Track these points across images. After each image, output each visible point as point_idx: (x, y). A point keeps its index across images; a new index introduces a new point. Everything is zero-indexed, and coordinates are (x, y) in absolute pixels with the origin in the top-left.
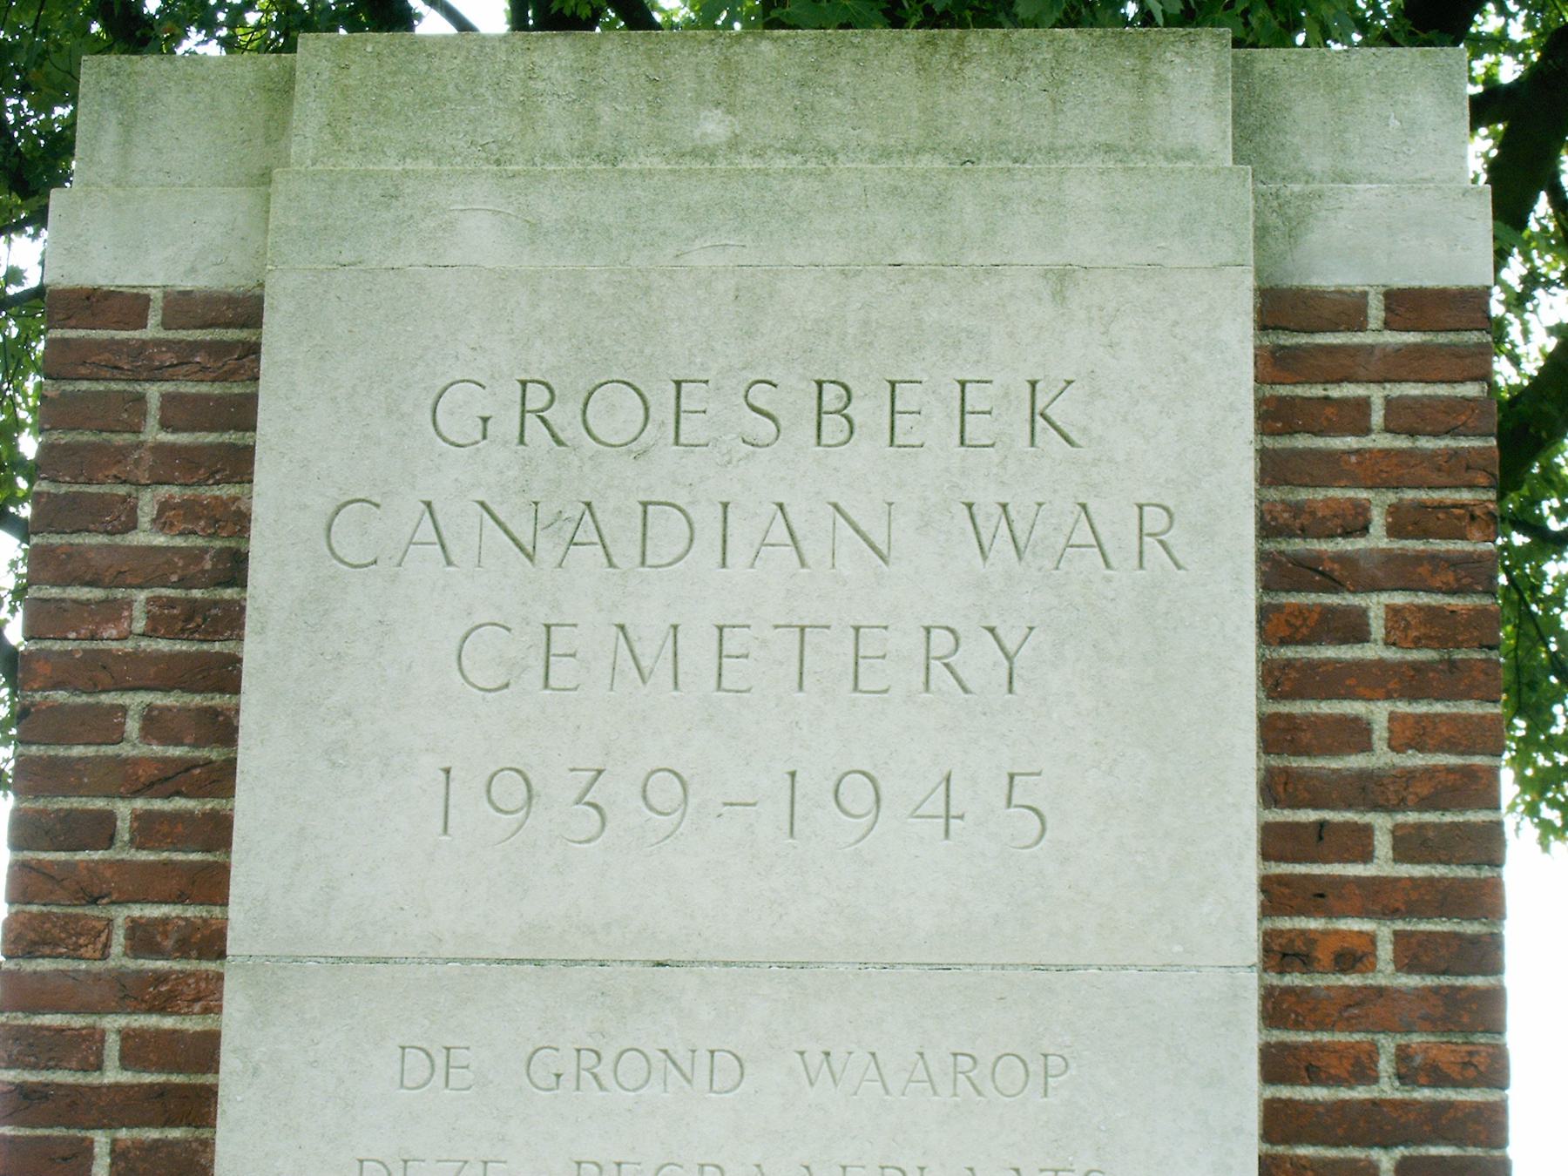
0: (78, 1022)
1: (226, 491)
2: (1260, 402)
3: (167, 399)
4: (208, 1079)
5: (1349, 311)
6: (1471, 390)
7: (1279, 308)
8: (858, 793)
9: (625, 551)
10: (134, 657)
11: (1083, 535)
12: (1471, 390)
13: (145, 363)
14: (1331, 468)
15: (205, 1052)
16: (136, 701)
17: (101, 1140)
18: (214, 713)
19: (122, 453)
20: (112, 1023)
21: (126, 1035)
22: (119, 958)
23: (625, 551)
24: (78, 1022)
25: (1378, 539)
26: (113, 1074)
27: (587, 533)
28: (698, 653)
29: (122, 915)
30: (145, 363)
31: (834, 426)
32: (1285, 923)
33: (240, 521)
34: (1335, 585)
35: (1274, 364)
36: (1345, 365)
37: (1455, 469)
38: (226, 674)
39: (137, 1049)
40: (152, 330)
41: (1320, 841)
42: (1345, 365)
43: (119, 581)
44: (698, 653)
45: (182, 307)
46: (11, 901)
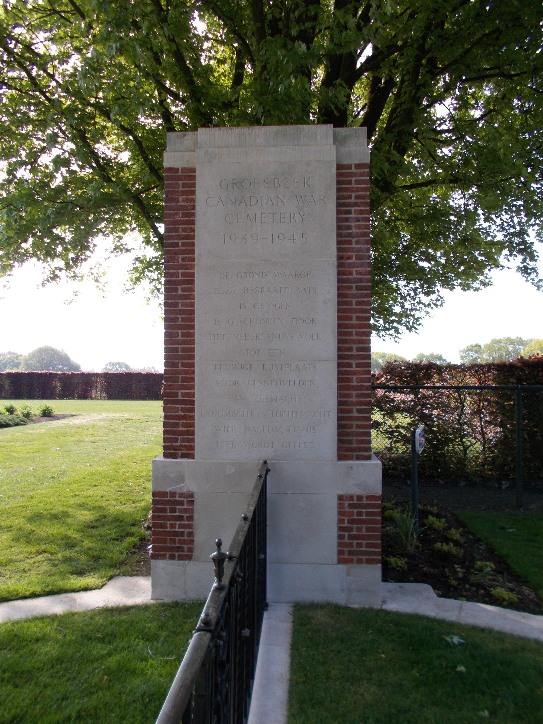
0: (175, 271)
1: (192, 196)
2: (338, 255)
3: (183, 184)
4: (193, 346)
5: (349, 167)
6: (367, 238)
7: (339, 167)
8: (281, 237)
9: (248, 204)
10: (180, 220)
11: (312, 199)
12: (367, 238)
13: (179, 178)
14: (347, 190)
15: (193, 275)
16: (181, 226)
17: (179, 287)
18: (191, 228)
19: (177, 191)
20: (180, 271)
21: (182, 273)
22: (180, 262)
23: (248, 204)
24: (175, 271)
25: (353, 195)
26: (180, 278)
27: (243, 201)
28: (259, 218)
29: (181, 256)
30: (179, 178)
31: (277, 185)
32: (342, 392)
33: (194, 200)
34: (347, 206)
35: (338, 175)
36: (350, 311)
37: (365, 204)
38: (193, 223)
39: (184, 275)
40: (180, 173)
41: (346, 242)
42: (350, 311)
43: (177, 210)
44: (259, 218)
45: (184, 169)
46: (165, 366)
